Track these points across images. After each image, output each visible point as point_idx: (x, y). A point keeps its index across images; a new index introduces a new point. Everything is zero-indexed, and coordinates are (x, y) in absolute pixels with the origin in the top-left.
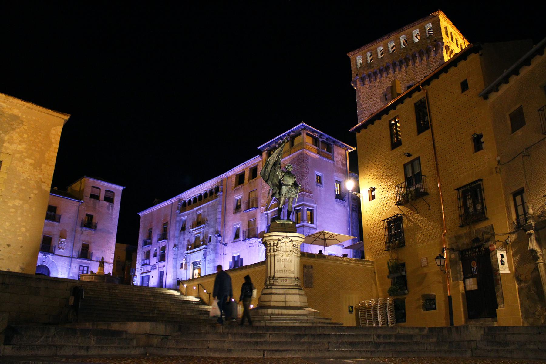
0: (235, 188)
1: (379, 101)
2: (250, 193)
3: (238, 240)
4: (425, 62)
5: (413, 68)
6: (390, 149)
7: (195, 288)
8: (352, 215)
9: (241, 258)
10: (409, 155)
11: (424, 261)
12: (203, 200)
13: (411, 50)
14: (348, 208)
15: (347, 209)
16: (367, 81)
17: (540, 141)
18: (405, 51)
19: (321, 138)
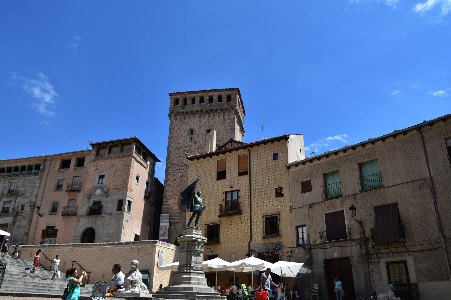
0: (58, 170)
1: (186, 133)
3: (55, 213)
4: (222, 117)
7: (372, 297)
8: (151, 208)
9: (56, 228)
10: (231, 187)
11: (233, 255)
12: (19, 172)
13: (215, 106)
14: (150, 203)
15: (149, 204)
16: (178, 117)
19: (143, 150)
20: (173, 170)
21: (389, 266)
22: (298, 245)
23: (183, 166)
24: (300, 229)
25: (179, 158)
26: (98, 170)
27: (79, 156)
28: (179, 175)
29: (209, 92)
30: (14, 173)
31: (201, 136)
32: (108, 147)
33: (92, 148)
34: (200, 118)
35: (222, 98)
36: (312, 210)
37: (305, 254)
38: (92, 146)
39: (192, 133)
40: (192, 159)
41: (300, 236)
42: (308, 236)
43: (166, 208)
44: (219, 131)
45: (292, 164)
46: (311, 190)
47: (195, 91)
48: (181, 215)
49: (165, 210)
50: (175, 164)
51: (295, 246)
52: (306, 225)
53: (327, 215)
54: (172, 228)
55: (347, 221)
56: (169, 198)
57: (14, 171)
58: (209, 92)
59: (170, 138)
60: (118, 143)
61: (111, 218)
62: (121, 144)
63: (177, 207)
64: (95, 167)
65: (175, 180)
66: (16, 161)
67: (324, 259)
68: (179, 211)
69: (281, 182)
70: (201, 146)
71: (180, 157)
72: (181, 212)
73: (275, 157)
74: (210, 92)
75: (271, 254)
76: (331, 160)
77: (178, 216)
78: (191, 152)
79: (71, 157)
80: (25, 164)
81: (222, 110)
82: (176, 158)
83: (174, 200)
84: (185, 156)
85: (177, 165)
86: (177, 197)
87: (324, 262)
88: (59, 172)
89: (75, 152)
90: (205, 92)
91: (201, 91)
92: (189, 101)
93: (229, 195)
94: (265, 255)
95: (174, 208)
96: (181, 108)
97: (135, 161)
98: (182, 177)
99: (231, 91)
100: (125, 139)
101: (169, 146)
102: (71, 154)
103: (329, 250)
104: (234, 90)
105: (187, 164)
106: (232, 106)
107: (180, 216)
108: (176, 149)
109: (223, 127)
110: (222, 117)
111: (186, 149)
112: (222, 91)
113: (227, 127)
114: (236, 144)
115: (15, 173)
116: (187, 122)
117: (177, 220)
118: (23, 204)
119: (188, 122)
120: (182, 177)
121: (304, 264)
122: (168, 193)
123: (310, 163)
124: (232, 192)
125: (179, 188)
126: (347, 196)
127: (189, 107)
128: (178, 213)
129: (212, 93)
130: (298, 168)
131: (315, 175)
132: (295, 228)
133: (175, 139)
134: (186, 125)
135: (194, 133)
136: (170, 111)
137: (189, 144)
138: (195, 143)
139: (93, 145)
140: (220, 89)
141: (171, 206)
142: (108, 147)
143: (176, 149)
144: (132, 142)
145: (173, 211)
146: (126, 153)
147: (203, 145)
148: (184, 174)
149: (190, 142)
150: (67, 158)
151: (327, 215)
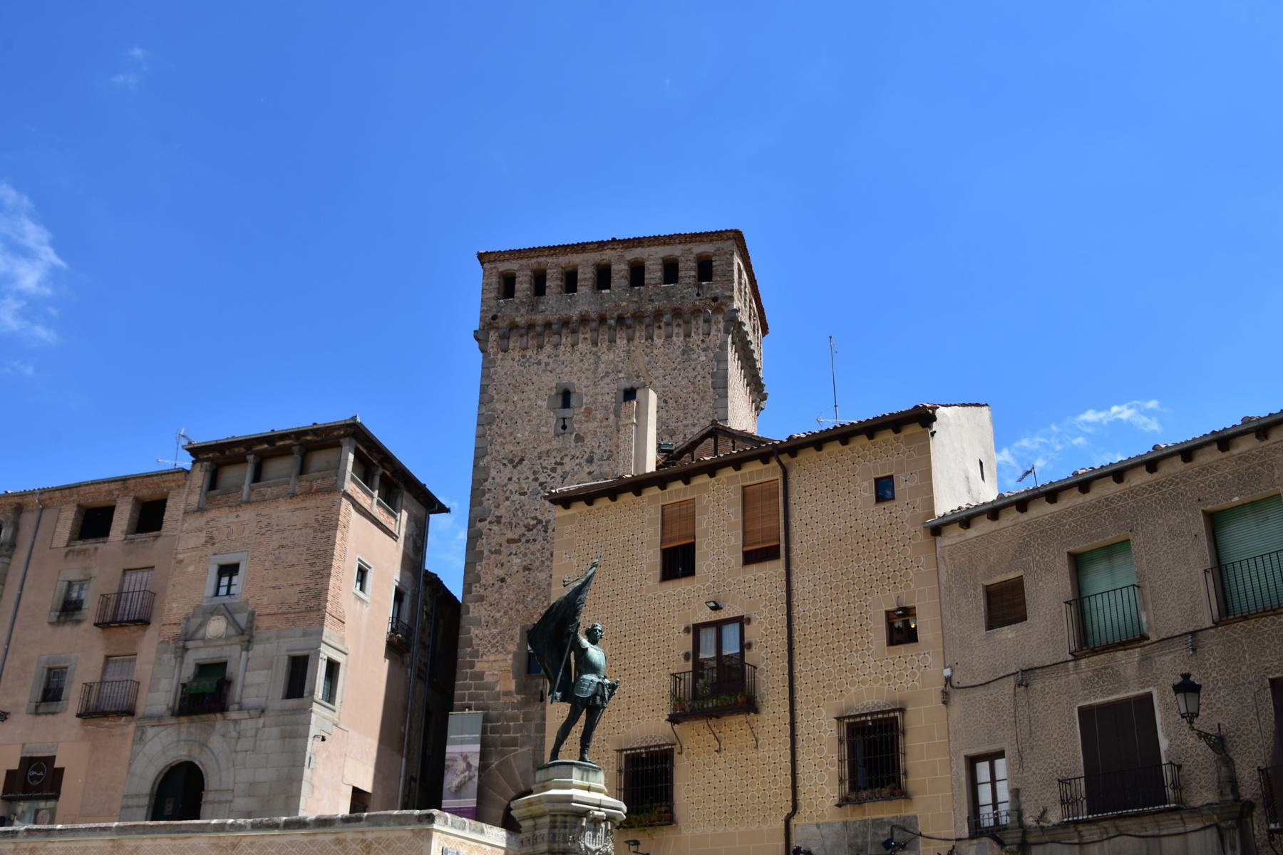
0: (68, 545)
1: (544, 404)
2: (125, 571)
4: (678, 340)
5: (647, 347)
6: (658, 577)
9: (57, 765)
13: (652, 301)
14: (409, 670)
15: (407, 673)
17: (1056, 664)
18: (636, 299)
20: (494, 542)
22: (977, 831)
23: (534, 526)
24: (983, 769)
25: (516, 497)
26: (213, 544)
27: (146, 493)
28: (516, 561)
29: (628, 248)
31: (599, 415)
32: (251, 458)
33: (194, 462)
34: (595, 343)
39: (566, 403)
40: (565, 501)
41: (985, 795)
43: (469, 687)
44: (670, 395)
46: (1024, 618)
48: (525, 714)
50: (503, 520)
51: (965, 832)
53: (1085, 713)
54: (493, 766)
55: (1167, 735)
59: (485, 421)
60: (288, 442)
61: (264, 727)
62: (298, 447)
63: (512, 685)
64: (203, 534)
65: (503, 580)
68: (519, 697)
69: (907, 586)
70: (601, 451)
72: (525, 703)
73: (884, 489)
76: (1099, 502)
77: (515, 719)
78: (564, 472)
81: (677, 313)
82: (507, 499)
83: (501, 657)
84: (539, 488)
85: (510, 523)
86: (513, 647)
88: (71, 554)
89: (129, 479)
92: (553, 284)
93: (708, 637)
95: (498, 689)
97: (353, 510)
98: (529, 569)
99: (711, 241)
100: (315, 427)
101: (480, 454)
102: (113, 486)
104: (724, 236)
105: (548, 522)
108: (504, 465)
109: (683, 378)
110: (678, 340)
111: (544, 464)
112: (677, 241)
113: (699, 378)
114: (733, 442)
116: (546, 360)
117: (511, 735)
119: (551, 361)
120: (529, 569)
122: (477, 632)
124: (718, 625)
125: (518, 611)
126: (1163, 640)
127: (554, 305)
129: (640, 248)
130: (972, 533)
131: (1038, 558)
133: (504, 425)
134: (545, 371)
135: (573, 402)
136: (482, 319)
137: (556, 444)
138: (579, 438)
139: (196, 451)
141: (488, 679)
143: (504, 465)
144: (342, 440)
145: (497, 697)
146: (318, 479)
147: (608, 449)
149: (557, 435)
150: (100, 500)
151: (1085, 713)
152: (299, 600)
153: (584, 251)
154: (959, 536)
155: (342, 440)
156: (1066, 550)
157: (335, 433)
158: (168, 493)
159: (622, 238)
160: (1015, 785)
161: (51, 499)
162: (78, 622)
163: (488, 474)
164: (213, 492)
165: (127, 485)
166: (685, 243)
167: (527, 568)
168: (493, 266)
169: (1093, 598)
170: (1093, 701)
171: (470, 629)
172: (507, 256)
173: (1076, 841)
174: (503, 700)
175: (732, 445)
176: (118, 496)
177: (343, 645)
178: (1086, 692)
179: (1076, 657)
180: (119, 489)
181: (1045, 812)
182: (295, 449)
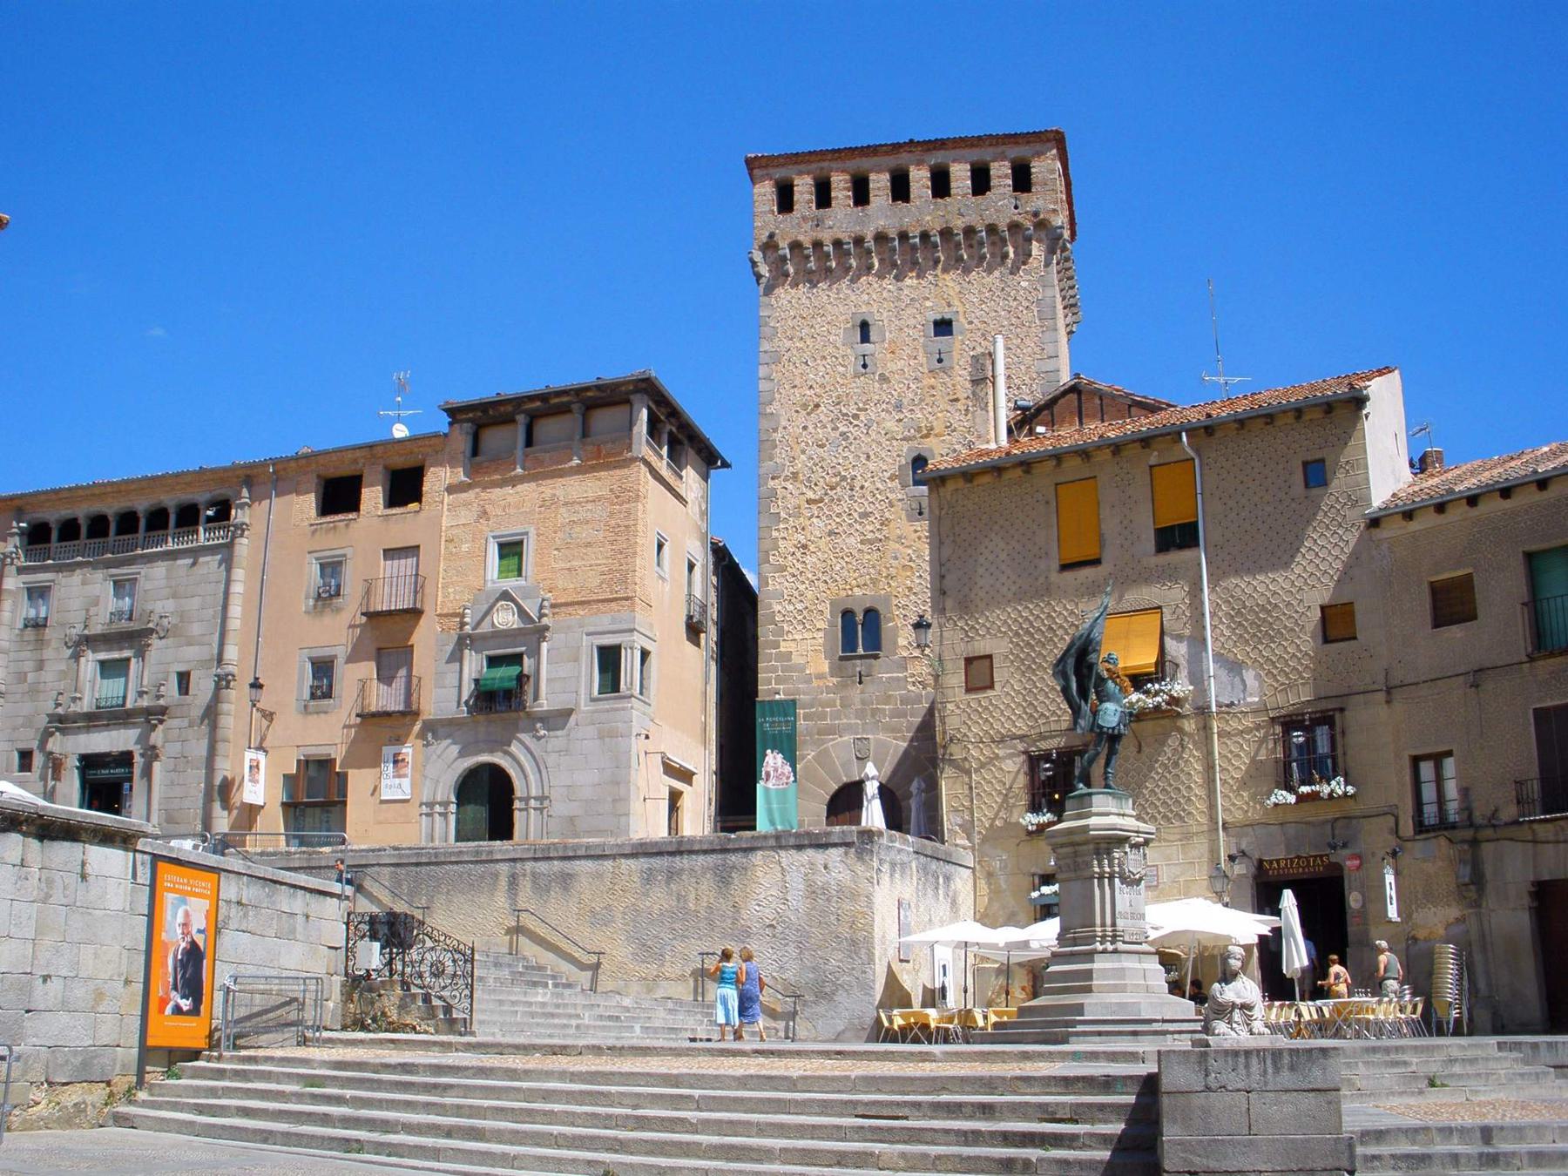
20: (791, 503)
21: (361, 493)
22: (1421, 827)
23: (837, 484)
24: (1427, 769)
27: (400, 462)
29: (929, 150)
30: (121, 537)
33: (451, 424)
35: (992, 177)
36: (1478, 694)
37: (1451, 861)
38: (449, 416)
39: (865, 338)
41: (1429, 792)
42: (1465, 792)
43: (775, 670)
45: (1391, 511)
46: (1474, 617)
47: (869, 146)
49: (885, 709)
52: (1455, 752)
53: (1541, 715)
56: (785, 625)
57: (120, 532)
58: (931, 147)
60: (565, 399)
62: (579, 405)
65: (805, 547)
66: (123, 488)
67: (1532, 879)
68: (835, 680)
71: (818, 446)
74: (935, 149)
75: (1309, 862)
76: (1558, 500)
77: (831, 704)
79: (361, 465)
80: (162, 498)
82: (803, 452)
87: (1530, 893)
88: (318, 533)
89: (377, 445)
90: (910, 152)
91: (893, 145)
94: (1283, 869)
95: (808, 672)
96: (807, 226)
97: (650, 477)
99: (1028, 142)
100: (600, 382)
102: (358, 454)
103: (1549, 849)
104: (1043, 137)
106: (1036, 214)
107: (838, 702)
111: (844, 411)
112: (987, 143)
115: (126, 537)
118: (182, 668)
121: (139, 730)
122: (779, 608)
123: (1467, 508)
128: (829, 690)
129: (942, 152)
130: (1414, 526)
131: (1489, 556)
132: (1407, 763)
135: (873, 336)
139: (454, 413)
140: (979, 137)
141: (796, 659)
142: (521, 419)
144: (632, 397)
145: (808, 679)
146: (607, 442)
148: (844, 521)
149: (857, 376)
150: (346, 471)
151: (1541, 715)
152: (602, 583)
153: (875, 155)
154: (1400, 528)
155: (632, 397)
156: (1521, 549)
157: (623, 388)
158: (424, 460)
159: (921, 140)
160: (1465, 785)
161: (285, 469)
162: (339, 610)
163: (778, 422)
164: (477, 459)
165: (375, 452)
166: (997, 144)
167: (831, 533)
168: (765, 172)
169: (1552, 602)
170: (1549, 703)
171: (771, 604)
172: (782, 160)
173: (1530, 838)
174: (815, 683)
175: (1099, 402)
176: (364, 464)
177: (652, 631)
178: (1542, 694)
179: (1531, 659)
180: (364, 457)
181: (1496, 810)
182: (575, 407)
